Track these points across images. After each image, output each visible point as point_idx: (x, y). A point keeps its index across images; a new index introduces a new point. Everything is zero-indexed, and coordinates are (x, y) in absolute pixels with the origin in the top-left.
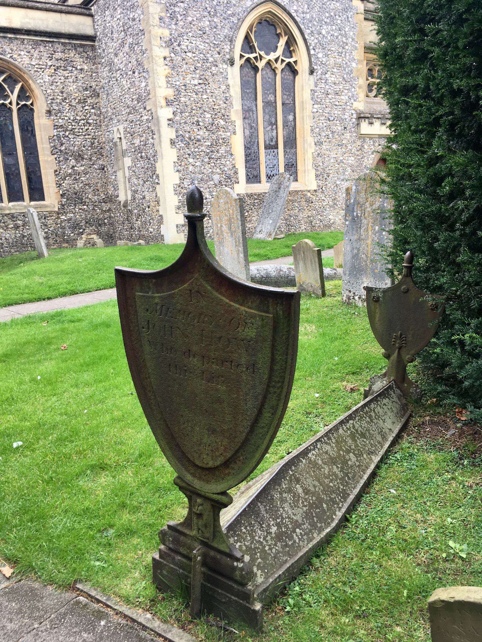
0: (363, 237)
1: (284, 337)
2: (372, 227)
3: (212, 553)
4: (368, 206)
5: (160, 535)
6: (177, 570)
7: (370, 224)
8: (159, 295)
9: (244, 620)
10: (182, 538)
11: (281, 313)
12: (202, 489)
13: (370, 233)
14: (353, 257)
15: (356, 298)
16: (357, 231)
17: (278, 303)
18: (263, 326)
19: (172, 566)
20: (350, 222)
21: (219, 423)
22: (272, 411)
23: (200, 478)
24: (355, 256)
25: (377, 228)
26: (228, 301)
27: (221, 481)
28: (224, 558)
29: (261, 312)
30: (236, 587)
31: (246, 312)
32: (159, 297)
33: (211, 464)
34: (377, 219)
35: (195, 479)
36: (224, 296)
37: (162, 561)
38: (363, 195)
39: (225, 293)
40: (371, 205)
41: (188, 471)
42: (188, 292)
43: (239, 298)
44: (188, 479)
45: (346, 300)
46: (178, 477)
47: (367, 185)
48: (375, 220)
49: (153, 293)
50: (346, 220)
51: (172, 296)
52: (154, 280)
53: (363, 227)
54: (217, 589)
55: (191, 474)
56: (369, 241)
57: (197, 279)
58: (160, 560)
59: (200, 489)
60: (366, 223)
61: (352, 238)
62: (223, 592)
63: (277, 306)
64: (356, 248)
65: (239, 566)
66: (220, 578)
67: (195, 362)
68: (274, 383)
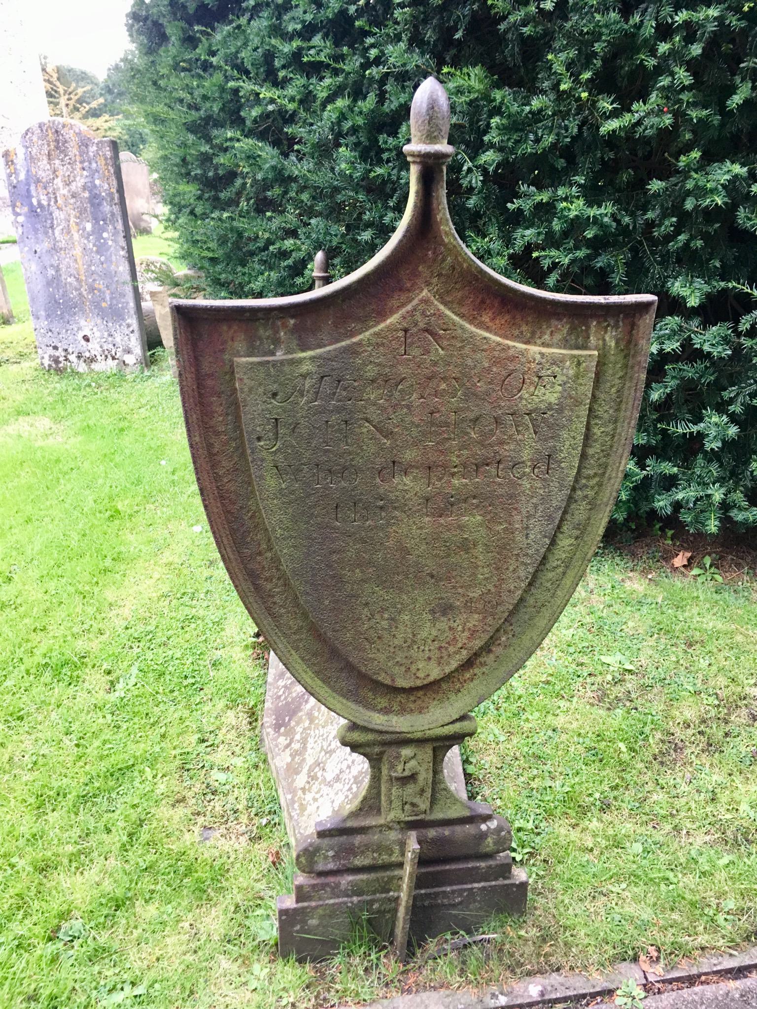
0: (62, 244)
1: (614, 390)
2: (77, 224)
3: (432, 833)
4: (61, 185)
5: (303, 860)
6: (345, 903)
7: (73, 220)
8: (310, 353)
9: (500, 910)
10: (358, 840)
11: (613, 344)
12: (415, 729)
13: (76, 236)
14: (49, 284)
15: (73, 358)
16: (46, 233)
17: (608, 326)
18: (577, 376)
19: (332, 901)
20: (26, 216)
21: (460, 590)
22: (576, 533)
23: (403, 711)
24: (54, 282)
25: (89, 226)
26: (498, 339)
27: (454, 697)
28: (458, 829)
29: (571, 348)
30: (483, 864)
31: (542, 355)
32: (312, 358)
33: (435, 673)
34: (85, 210)
35: (391, 716)
36: (488, 329)
37: (305, 904)
38: (44, 163)
39: (490, 324)
40: (68, 184)
41: (372, 708)
42: (401, 334)
43: (524, 328)
44: (378, 722)
45: (50, 366)
46: (354, 726)
47: (49, 145)
48: (82, 211)
49: (288, 352)
50: (17, 214)
51: (353, 351)
52: (292, 322)
53: (58, 225)
54: (444, 889)
55: (380, 711)
56: (78, 251)
57: (426, 301)
58: (300, 905)
59: (410, 729)
60: (62, 217)
61: (38, 248)
62: (455, 887)
63: (606, 332)
64: (52, 266)
65: (492, 827)
66: (448, 867)
67: (408, 485)
68: (584, 481)
